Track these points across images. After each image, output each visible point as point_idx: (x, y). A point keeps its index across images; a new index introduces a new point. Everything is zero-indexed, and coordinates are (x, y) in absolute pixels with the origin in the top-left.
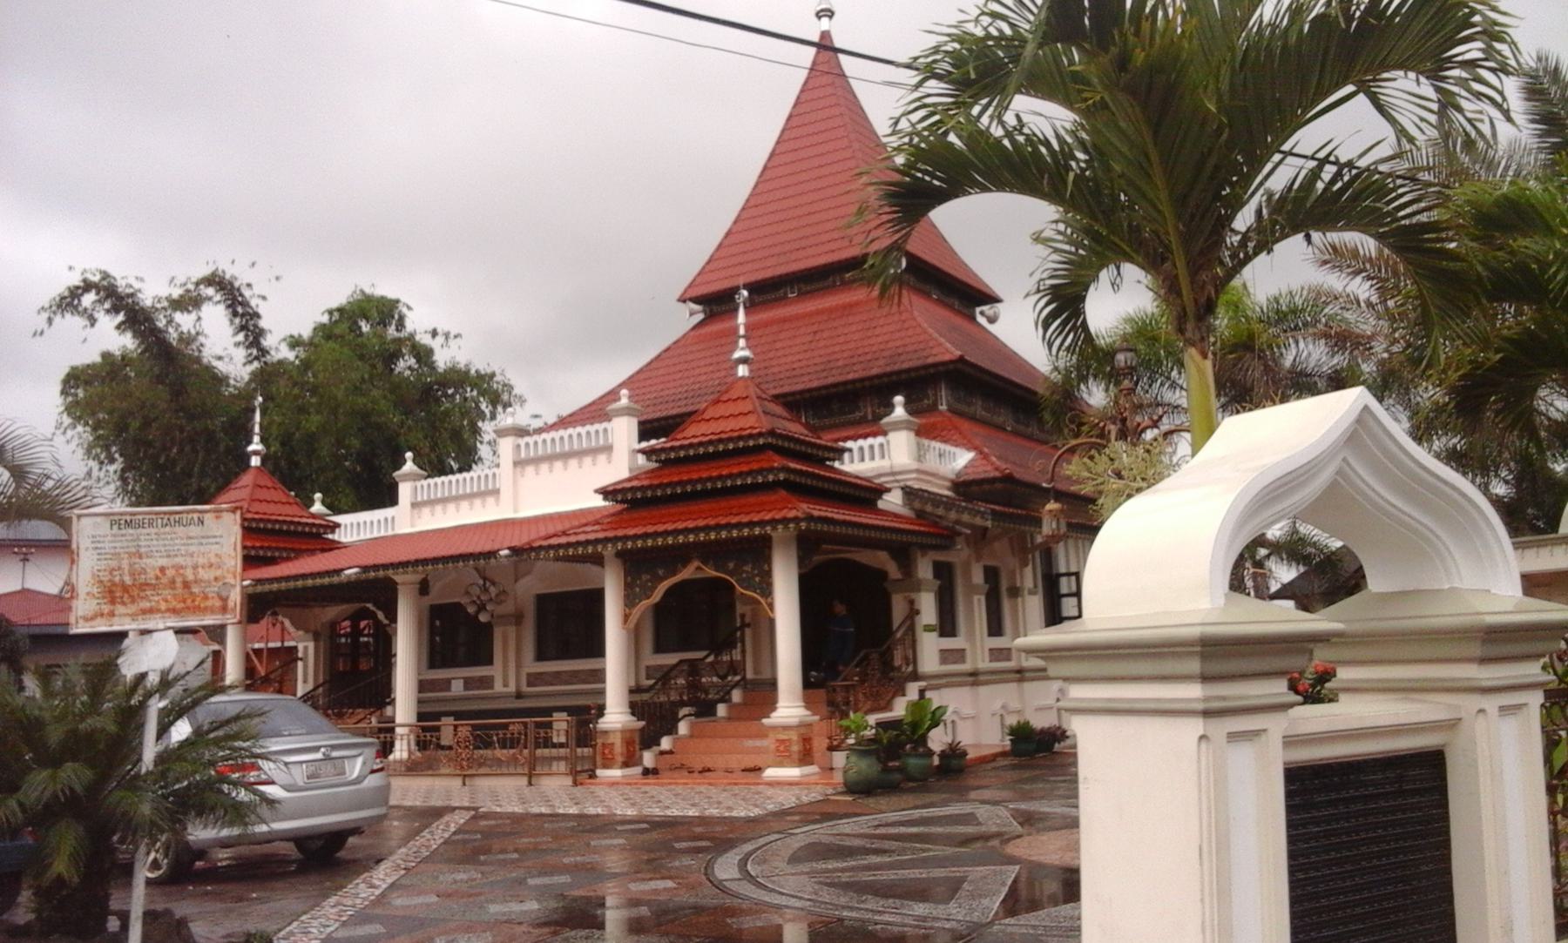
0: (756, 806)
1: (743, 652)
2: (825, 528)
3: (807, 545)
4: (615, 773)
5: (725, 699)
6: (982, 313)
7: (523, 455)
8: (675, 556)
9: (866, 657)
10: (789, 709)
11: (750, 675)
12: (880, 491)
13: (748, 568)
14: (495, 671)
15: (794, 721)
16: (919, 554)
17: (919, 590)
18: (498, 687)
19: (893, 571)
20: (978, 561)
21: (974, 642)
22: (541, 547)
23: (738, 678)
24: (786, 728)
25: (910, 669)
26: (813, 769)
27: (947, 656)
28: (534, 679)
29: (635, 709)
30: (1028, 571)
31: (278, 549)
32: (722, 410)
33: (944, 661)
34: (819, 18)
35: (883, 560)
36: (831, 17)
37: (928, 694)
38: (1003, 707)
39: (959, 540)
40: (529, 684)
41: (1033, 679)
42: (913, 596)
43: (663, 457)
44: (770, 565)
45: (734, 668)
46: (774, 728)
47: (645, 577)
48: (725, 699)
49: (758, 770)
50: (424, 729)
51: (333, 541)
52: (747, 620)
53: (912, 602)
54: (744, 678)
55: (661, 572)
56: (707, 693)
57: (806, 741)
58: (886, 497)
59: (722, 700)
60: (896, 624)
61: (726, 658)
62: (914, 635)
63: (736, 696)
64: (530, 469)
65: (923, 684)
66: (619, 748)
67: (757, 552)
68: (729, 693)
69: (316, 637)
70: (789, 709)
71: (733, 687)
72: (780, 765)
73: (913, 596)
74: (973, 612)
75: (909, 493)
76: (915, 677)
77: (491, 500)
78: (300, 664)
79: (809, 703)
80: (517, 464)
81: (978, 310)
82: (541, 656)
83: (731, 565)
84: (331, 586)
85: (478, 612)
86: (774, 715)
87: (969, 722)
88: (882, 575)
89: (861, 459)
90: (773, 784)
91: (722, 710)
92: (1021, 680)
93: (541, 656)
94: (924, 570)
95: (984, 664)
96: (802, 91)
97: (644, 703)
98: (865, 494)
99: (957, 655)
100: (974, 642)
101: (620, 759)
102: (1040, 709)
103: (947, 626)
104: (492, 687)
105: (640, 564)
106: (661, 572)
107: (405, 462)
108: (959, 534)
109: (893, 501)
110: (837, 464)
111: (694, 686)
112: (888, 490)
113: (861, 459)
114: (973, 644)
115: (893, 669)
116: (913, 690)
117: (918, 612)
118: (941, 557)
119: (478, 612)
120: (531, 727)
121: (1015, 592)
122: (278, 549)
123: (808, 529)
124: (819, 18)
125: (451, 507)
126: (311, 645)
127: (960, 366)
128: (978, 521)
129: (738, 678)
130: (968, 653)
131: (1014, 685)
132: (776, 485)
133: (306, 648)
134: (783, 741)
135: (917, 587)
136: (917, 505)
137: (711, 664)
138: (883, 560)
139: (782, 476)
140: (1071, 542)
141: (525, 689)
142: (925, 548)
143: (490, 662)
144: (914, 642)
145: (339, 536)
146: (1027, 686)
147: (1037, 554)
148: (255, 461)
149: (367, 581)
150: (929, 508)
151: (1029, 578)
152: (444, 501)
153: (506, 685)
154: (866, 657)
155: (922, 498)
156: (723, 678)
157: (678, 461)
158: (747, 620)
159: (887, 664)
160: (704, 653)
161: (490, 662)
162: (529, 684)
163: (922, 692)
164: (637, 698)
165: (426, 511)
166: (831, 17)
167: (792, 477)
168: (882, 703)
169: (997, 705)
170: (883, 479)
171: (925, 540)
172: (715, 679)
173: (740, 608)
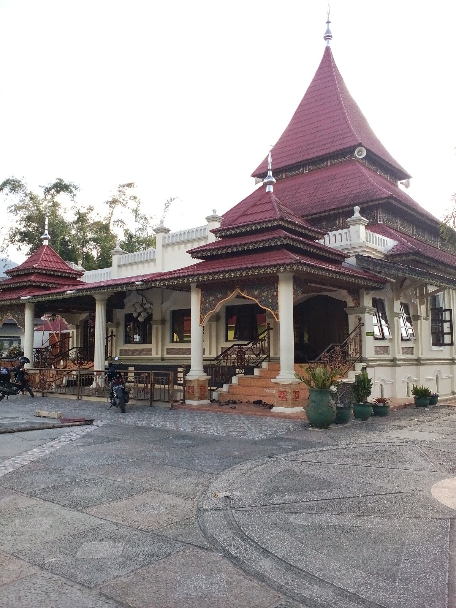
0: (260, 432)
1: (269, 342)
2: (309, 270)
3: (300, 281)
4: (195, 403)
5: (259, 366)
6: (402, 183)
7: (167, 242)
8: (226, 286)
9: (333, 347)
10: (287, 372)
11: (272, 355)
12: (345, 257)
13: (265, 294)
14: (151, 346)
15: (289, 382)
17: (364, 313)
18: (154, 355)
19: (350, 302)
20: (398, 299)
22: (157, 280)
23: (265, 356)
24: (284, 385)
28: (170, 351)
29: (206, 369)
30: (423, 307)
31: (50, 283)
32: (256, 209)
33: (377, 352)
35: (343, 295)
37: (368, 370)
39: (388, 285)
40: (168, 354)
41: (400, 365)
42: (361, 316)
43: (223, 234)
44: (277, 292)
45: (263, 351)
46: (277, 384)
47: (211, 298)
48: (259, 366)
49: (271, 407)
51: (80, 281)
52: (271, 326)
53: (360, 320)
54: (269, 356)
55: (219, 296)
56: (248, 362)
57: (296, 393)
58: (348, 260)
59: (257, 367)
60: (350, 330)
61: (259, 345)
62: (360, 338)
63: (265, 365)
64: (170, 249)
65: (365, 364)
66: (197, 389)
67: (271, 282)
68: (260, 363)
69: (77, 327)
71: (263, 360)
72: (281, 405)
73: (361, 316)
75: (360, 258)
76: (362, 360)
77: (152, 264)
78: (70, 339)
80: (164, 246)
81: (399, 182)
83: (256, 293)
84: (60, 300)
85: (138, 317)
88: (344, 304)
89: (333, 240)
90: (279, 416)
91: (256, 372)
92: (394, 365)
94: (367, 302)
95: (400, 356)
97: (212, 367)
98: (336, 257)
101: (197, 395)
102: (427, 380)
104: (151, 354)
105: (209, 289)
106: (219, 296)
108: (389, 282)
109: (352, 261)
110: (321, 242)
111: (241, 359)
112: (349, 257)
113: (333, 240)
115: (348, 355)
116: (359, 366)
117: (363, 325)
118: (379, 295)
119: (138, 317)
120: (152, 375)
122: (50, 283)
123: (298, 269)
125: (135, 267)
126: (75, 331)
127: (390, 200)
128: (400, 274)
129: (265, 356)
130: (390, 349)
131: (448, 366)
132: (283, 246)
133: (73, 332)
134: (282, 392)
135: (364, 310)
136: (365, 265)
137: (251, 348)
138: (343, 295)
139: (285, 242)
140: (446, 291)
141: (166, 356)
142: (368, 289)
143: (151, 342)
144: (361, 341)
145: (82, 279)
146: (422, 368)
147: (429, 299)
148: (46, 243)
149: (79, 298)
150: (371, 267)
152: (132, 264)
153: (157, 354)
154: (333, 347)
155: (368, 261)
156: (257, 355)
157: (231, 236)
158: (271, 326)
159: (345, 352)
160: (246, 343)
161: (151, 342)
162: (168, 354)
164: (208, 363)
165: (124, 269)
167: (291, 243)
170: (346, 252)
171: (368, 283)
172: (253, 356)
173: (268, 320)
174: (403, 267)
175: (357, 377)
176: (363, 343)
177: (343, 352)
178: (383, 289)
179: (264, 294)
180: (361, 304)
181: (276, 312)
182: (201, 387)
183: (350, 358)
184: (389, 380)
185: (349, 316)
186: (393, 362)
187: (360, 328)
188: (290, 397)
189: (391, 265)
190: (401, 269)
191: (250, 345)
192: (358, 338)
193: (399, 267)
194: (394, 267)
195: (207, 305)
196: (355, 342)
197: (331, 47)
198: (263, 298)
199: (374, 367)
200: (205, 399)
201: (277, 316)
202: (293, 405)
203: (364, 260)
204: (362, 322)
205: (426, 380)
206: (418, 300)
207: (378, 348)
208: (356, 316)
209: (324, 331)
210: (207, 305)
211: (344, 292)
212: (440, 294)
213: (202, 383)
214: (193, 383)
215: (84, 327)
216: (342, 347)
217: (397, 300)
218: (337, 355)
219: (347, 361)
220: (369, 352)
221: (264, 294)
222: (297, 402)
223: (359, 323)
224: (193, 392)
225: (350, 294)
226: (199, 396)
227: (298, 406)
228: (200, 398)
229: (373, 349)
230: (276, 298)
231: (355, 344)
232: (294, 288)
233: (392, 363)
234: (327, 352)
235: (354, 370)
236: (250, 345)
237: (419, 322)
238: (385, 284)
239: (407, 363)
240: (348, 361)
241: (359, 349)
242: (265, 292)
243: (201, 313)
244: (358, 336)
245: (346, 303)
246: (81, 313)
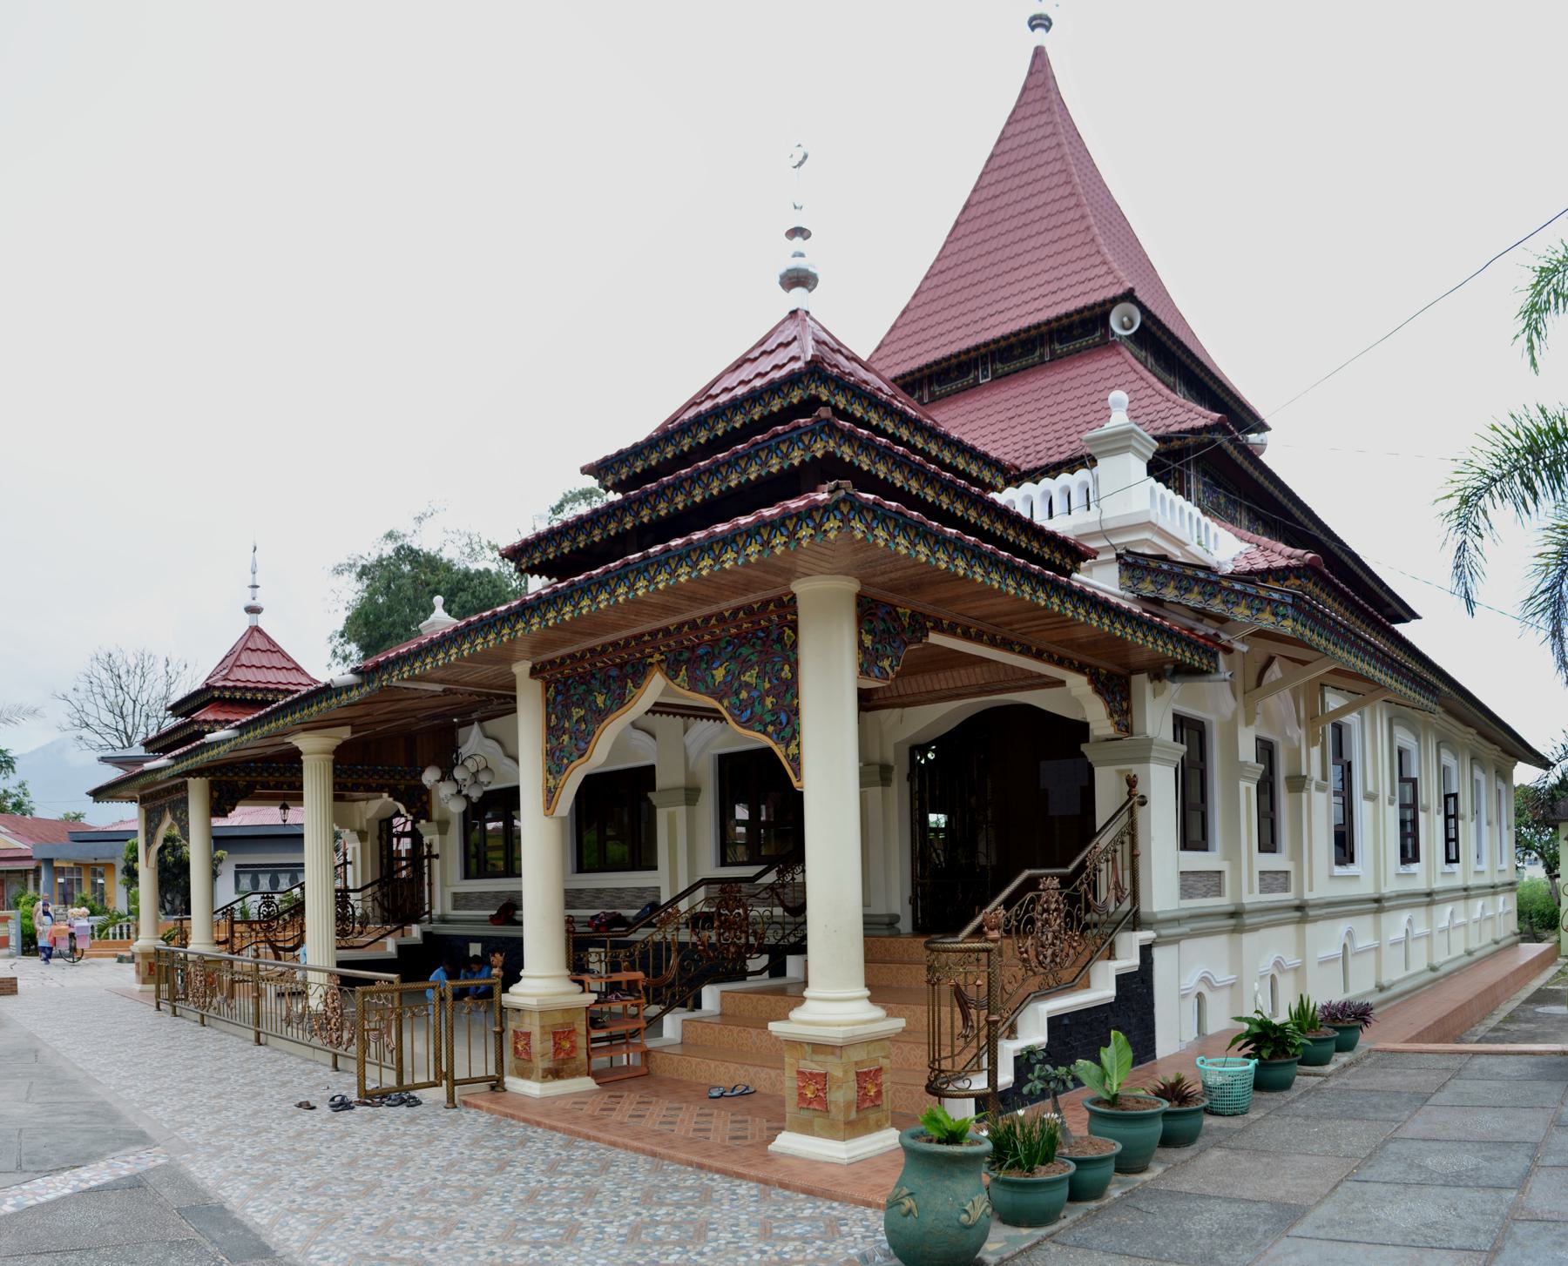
9: (1032, 884)
10: (835, 1000)
16: (1149, 687)
17: (1145, 760)
20: (1248, 723)
21: (1236, 856)
25: (1126, 906)
26: (887, 1139)
27: (1191, 883)
34: (1033, 28)
35: (1077, 697)
36: (1048, 28)
37: (1157, 953)
38: (1277, 964)
41: (1255, 928)
42: (1135, 769)
43: (624, 473)
46: (794, 1044)
47: (577, 713)
50: (346, 981)
53: (1132, 782)
60: (1101, 819)
65: (1146, 935)
66: (540, 1046)
69: (362, 836)
70: (835, 1000)
72: (805, 1128)
73: (1135, 769)
74: (1234, 804)
79: (879, 992)
82: (467, 875)
86: (795, 1014)
87: (1225, 993)
88: (1080, 730)
93: (467, 875)
95: (1252, 897)
96: (1008, 124)
99: (1212, 881)
100: (1236, 856)
101: (541, 1064)
103: (1194, 834)
107: (433, 610)
114: (1236, 867)
117: (1143, 802)
121: (1298, 783)
124: (1033, 28)
135: (1143, 753)
136: (1147, 588)
138: (1077, 697)
142: (1161, 672)
143: (652, 866)
150: (1170, 594)
151: (1313, 762)
163: (1146, 951)
166: (1048, 28)
168: (1066, 975)
169: (1266, 965)
172: (778, 911)
174: (1276, 596)
175: (1122, 980)
176: (1141, 861)
177: (1073, 900)
178: (1207, 673)
179: (746, 678)
180: (1136, 729)
181: (792, 749)
182: (555, 1034)
183: (1096, 917)
184: (1222, 976)
185: (1098, 771)
186: (1236, 919)
187: (1132, 812)
188: (842, 1095)
189: (1238, 587)
190: (1270, 601)
191: (771, 878)
192: (1127, 846)
193: (1263, 593)
194: (1244, 594)
195: (566, 738)
196: (1114, 860)
197: (1048, 50)
198: (744, 695)
199: (1177, 942)
200: (574, 1074)
201: (796, 761)
202: (853, 1128)
203: (1147, 569)
204: (1140, 790)
205: (1320, 963)
206: (1302, 732)
207: (1192, 878)
208: (1120, 772)
209: (1001, 828)
210: (566, 738)
211: (1078, 684)
212: (1352, 719)
213: (559, 1019)
214: (527, 1020)
215: (380, 838)
216: (1066, 881)
217: (1247, 725)
218: (1044, 911)
219: (1089, 921)
220: (1162, 891)
221: (746, 678)
222: (873, 1116)
223: (1131, 794)
224: (528, 1053)
225: (1097, 691)
226: (547, 1064)
227: (879, 1127)
228: (555, 1073)
229: (1174, 884)
230: (791, 687)
231: (1115, 868)
232: (861, 644)
233: (1232, 922)
234: (1008, 904)
235: (1111, 956)
236: (771, 878)
237: (1304, 795)
238: (1215, 656)
239: (1271, 916)
240: (1087, 926)
241: (1127, 885)
242: (751, 667)
243: (549, 771)
244: (1127, 839)
245: (1086, 725)
246: (368, 800)
